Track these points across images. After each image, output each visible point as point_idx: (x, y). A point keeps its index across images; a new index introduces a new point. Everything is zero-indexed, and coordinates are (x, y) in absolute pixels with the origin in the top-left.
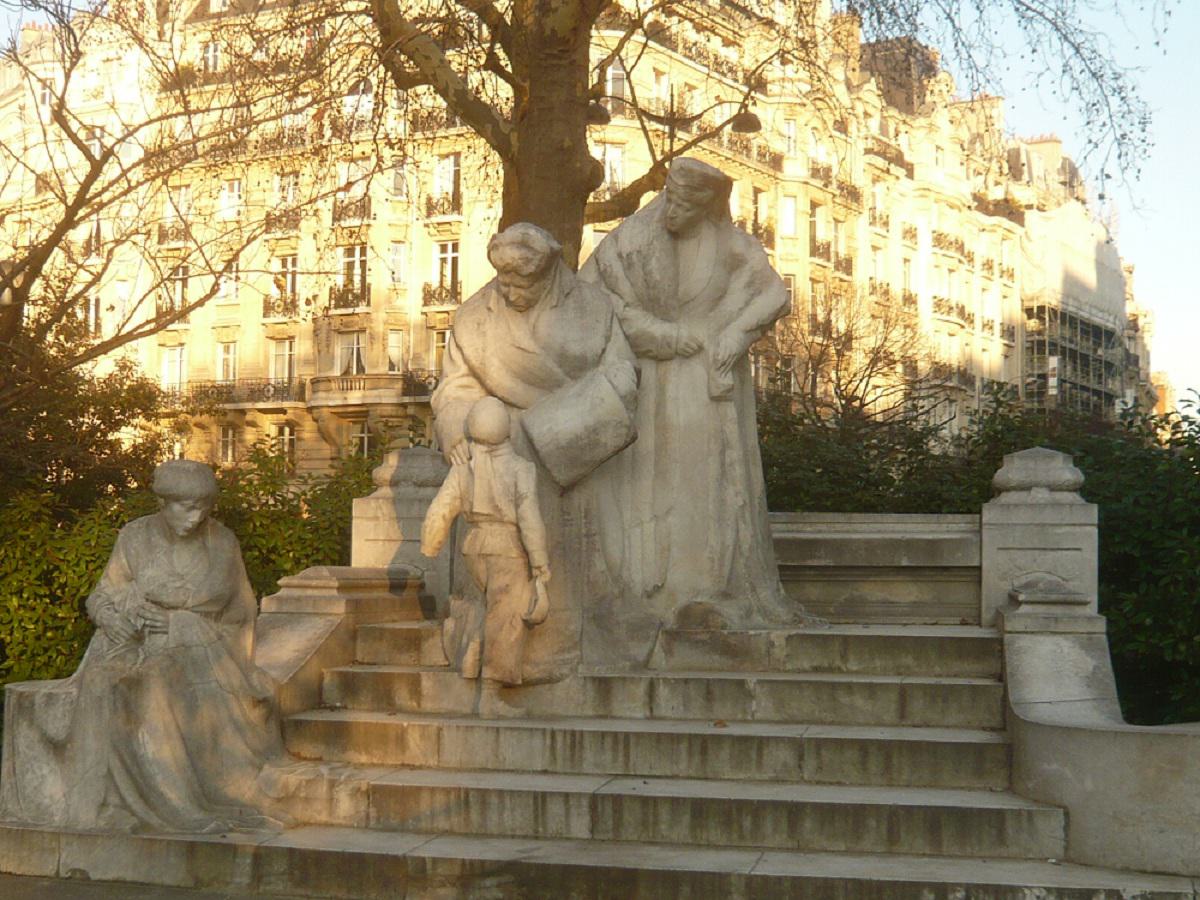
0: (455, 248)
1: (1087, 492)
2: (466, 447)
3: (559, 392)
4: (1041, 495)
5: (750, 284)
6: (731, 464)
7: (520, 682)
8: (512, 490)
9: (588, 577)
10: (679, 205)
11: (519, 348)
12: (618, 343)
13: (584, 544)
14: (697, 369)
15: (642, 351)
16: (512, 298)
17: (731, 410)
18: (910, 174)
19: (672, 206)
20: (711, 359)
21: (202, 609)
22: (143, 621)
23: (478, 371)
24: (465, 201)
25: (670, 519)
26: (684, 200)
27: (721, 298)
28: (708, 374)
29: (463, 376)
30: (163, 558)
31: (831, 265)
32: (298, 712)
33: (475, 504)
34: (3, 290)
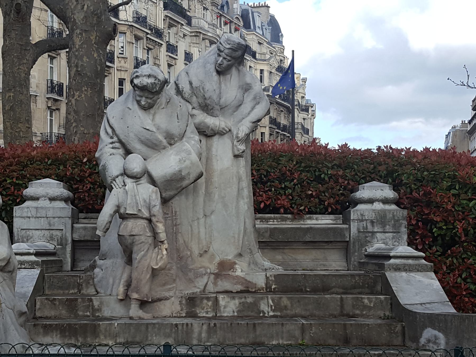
1: (360, 150)
2: (122, 181)
4: (378, 206)
5: (255, 98)
6: (242, 189)
7: (150, 300)
8: (148, 201)
9: (176, 246)
10: (224, 58)
12: (191, 128)
13: (175, 229)
14: (226, 140)
15: (206, 133)
16: (143, 103)
17: (242, 161)
19: (221, 58)
20: (235, 136)
23: (123, 141)
25: (213, 217)
26: (227, 55)
27: (240, 105)
28: (233, 144)
33: (128, 208)
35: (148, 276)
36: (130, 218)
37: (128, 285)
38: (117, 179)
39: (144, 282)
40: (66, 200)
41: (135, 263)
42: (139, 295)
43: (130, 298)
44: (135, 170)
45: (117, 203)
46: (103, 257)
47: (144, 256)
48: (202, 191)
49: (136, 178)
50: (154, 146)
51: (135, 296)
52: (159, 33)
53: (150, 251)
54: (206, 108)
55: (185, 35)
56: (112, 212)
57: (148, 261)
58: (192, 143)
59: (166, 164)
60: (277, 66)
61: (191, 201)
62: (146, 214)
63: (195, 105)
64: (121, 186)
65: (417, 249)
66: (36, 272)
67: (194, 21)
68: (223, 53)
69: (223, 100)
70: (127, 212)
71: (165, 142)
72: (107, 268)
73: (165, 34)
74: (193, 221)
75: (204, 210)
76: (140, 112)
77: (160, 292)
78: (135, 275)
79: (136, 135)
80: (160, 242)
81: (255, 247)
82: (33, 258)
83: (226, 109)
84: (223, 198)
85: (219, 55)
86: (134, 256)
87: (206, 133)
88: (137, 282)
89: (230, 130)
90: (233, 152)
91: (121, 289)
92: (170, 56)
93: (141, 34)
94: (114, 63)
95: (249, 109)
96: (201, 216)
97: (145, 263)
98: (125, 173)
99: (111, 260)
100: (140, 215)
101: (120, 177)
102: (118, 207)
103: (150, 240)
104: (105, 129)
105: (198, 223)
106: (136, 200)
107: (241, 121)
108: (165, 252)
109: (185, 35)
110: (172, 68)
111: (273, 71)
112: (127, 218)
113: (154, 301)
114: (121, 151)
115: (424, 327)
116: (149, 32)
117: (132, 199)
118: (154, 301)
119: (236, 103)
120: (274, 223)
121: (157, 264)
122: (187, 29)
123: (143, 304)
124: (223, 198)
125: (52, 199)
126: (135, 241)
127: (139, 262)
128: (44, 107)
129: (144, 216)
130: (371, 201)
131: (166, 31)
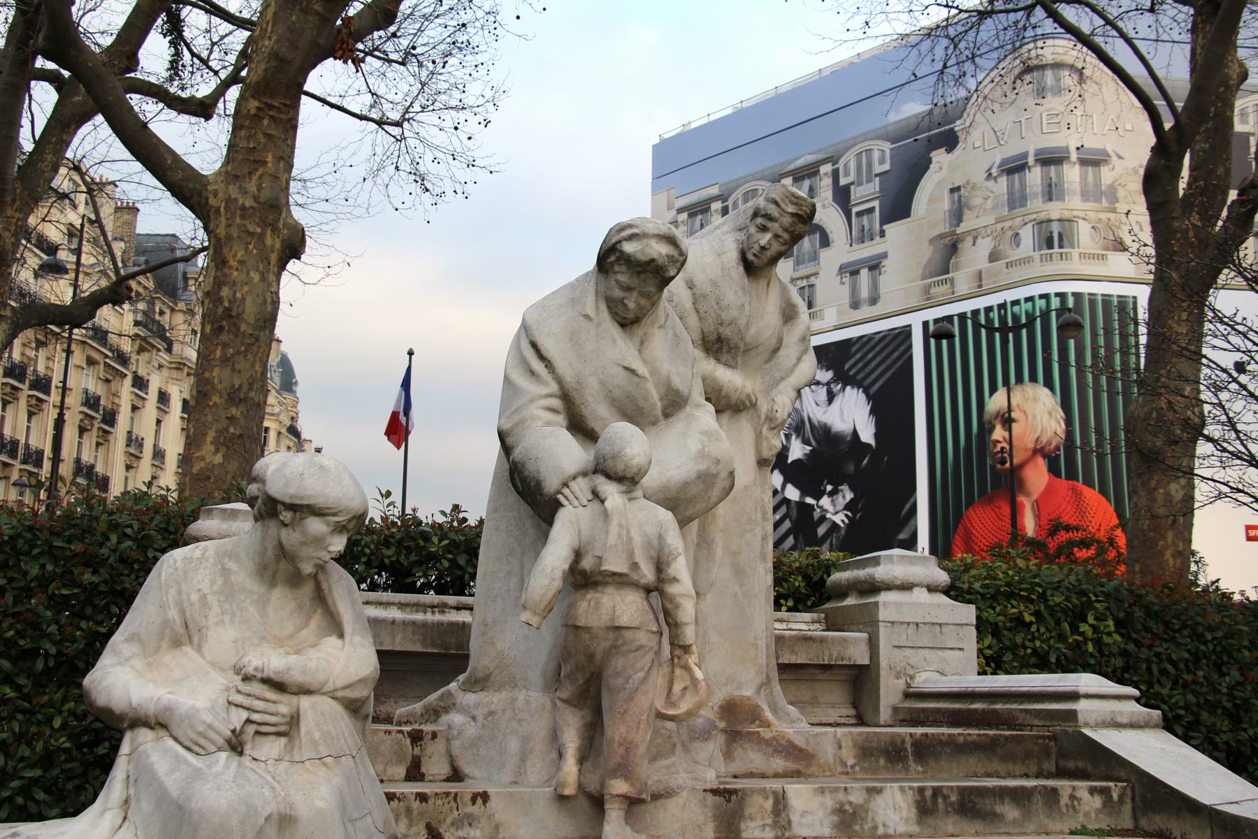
4: (920, 595)
8: (655, 543)
11: (626, 368)
18: (169, 350)
19: (768, 236)
21: (340, 694)
22: (245, 715)
29: (551, 396)
30: (252, 610)
31: (99, 417)
34: (18, 92)
36: (606, 584)
38: (573, 484)
42: (632, 785)
45: (576, 545)
46: (479, 683)
52: (123, 359)
53: (654, 670)
55: (160, 366)
57: (650, 695)
60: (288, 423)
64: (585, 503)
67: (176, 348)
68: (776, 225)
69: (753, 331)
70: (603, 568)
72: (492, 713)
73: (132, 361)
76: (614, 330)
79: (602, 383)
80: (680, 647)
81: (775, 674)
83: (753, 353)
84: (735, 554)
90: (758, 451)
92: (137, 395)
93: (96, 356)
94: (48, 394)
95: (794, 361)
99: (504, 694)
100: (634, 576)
101: (580, 479)
102: (578, 555)
106: (630, 539)
107: (776, 383)
109: (160, 366)
110: (138, 413)
111: (284, 431)
116: (110, 354)
117: (620, 536)
118: (656, 797)
122: (164, 357)
124: (735, 554)
126: (620, 642)
130: (906, 587)
131: (134, 357)
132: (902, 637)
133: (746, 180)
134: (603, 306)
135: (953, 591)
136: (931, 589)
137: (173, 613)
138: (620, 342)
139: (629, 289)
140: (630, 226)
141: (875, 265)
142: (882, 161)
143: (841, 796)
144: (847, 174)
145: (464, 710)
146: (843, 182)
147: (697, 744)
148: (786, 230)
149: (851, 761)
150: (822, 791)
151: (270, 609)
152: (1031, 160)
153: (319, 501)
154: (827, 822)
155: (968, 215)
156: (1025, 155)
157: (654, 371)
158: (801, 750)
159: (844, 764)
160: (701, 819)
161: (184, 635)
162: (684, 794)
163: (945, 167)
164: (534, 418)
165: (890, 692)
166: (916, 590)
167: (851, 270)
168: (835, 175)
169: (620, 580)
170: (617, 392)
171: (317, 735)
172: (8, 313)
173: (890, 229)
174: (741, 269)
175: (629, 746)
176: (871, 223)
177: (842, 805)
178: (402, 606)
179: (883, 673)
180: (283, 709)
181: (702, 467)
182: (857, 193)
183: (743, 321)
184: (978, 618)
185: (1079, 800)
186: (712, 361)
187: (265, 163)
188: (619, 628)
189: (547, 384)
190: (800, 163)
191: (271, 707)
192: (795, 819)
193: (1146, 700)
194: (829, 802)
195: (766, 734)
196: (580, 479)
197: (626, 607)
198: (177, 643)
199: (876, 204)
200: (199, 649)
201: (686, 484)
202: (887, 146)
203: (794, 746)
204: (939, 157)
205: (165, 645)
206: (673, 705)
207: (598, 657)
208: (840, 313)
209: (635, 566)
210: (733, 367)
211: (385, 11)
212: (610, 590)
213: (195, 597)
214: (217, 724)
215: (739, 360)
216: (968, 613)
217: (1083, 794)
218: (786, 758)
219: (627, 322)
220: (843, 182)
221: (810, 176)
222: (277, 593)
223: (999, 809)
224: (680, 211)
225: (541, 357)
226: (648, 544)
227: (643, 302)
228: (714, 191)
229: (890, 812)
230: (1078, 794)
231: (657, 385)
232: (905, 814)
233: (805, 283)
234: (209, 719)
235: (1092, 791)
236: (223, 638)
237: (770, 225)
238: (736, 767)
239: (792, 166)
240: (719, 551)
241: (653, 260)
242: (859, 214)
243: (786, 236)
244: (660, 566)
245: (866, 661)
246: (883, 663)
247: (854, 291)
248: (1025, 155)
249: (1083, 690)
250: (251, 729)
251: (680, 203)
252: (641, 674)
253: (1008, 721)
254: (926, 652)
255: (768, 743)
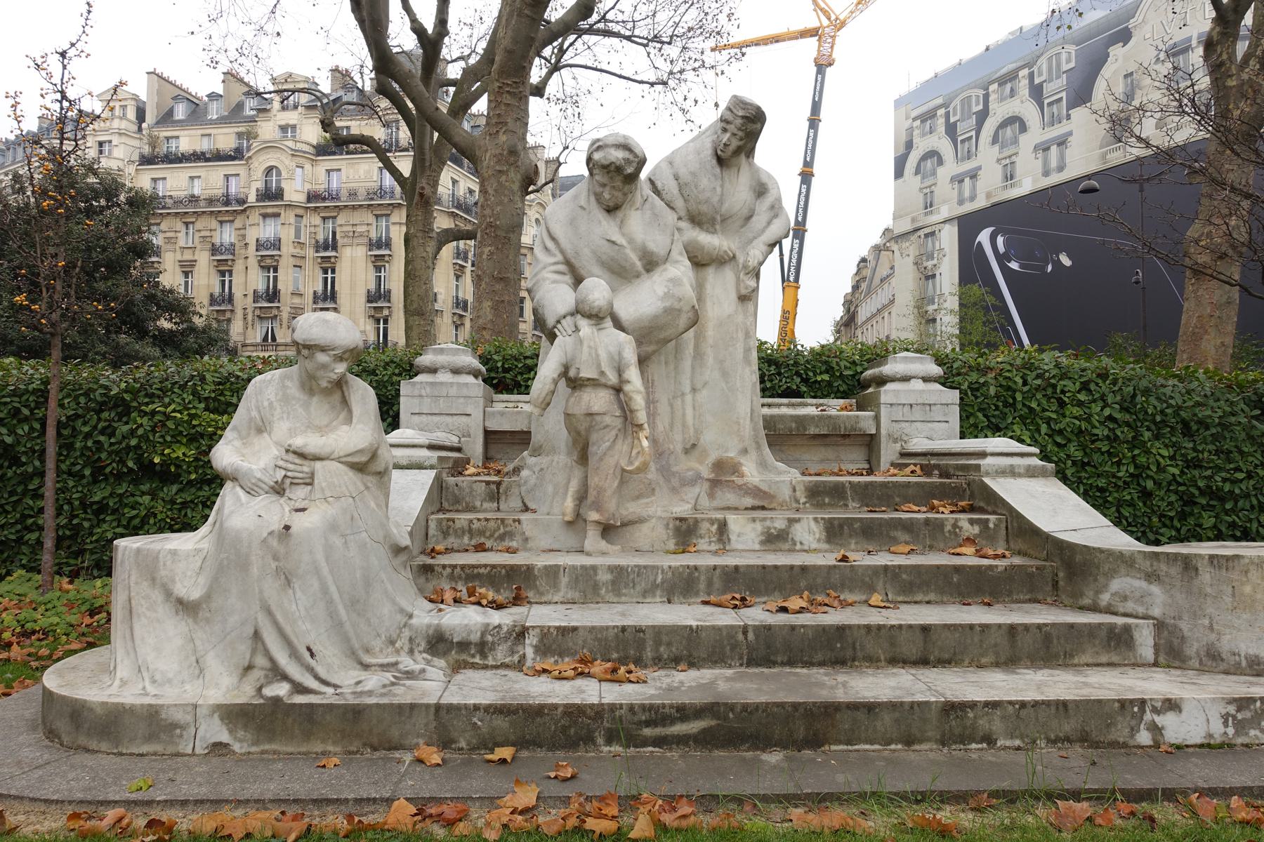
0: (333, 271)
3: (637, 281)
4: (917, 385)
8: (616, 357)
10: (734, 135)
12: (678, 249)
14: (728, 274)
19: (728, 135)
21: (349, 459)
22: (283, 473)
24: (339, 245)
25: (705, 392)
27: (751, 217)
30: (300, 410)
32: (1122, 561)
35: (616, 484)
37: (581, 498)
38: (563, 322)
39: (609, 492)
40: (476, 374)
41: (592, 461)
43: (585, 521)
44: (596, 304)
45: (564, 361)
46: (537, 452)
47: (610, 448)
48: (689, 350)
49: (596, 317)
50: (620, 273)
51: (594, 516)
53: (620, 442)
54: (696, 220)
56: (556, 376)
58: (680, 269)
59: (641, 301)
61: (672, 367)
62: (612, 378)
63: (683, 213)
65: (1021, 441)
66: (428, 477)
69: (726, 206)
71: (639, 264)
74: (674, 397)
75: (692, 382)
76: (600, 215)
77: (633, 509)
78: (594, 481)
79: (594, 252)
82: (425, 453)
83: (729, 221)
85: (725, 130)
86: (592, 449)
87: (700, 261)
88: (599, 493)
89: (734, 257)
90: (738, 290)
91: (569, 504)
96: (688, 389)
97: (610, 461)
98: (578, 311)
100: (603, 380)
101: (568, 318)
102: (566, 368)
103: (618, 423)
104: (543, 242)
105: (683, 401)
106: (598, 356)
107: (751, 241)
108: (645, 443)
112: (582, 386)
113: (624, 525)
114: (568, 278)
115: (1112, 574)
118: (624, 525)
119: (745, 212)
120: (785, 409)
121: (631, 463)
123: (607, 530)
124: (722, 362)
125: (456, 371)
127: (601, 459)
128: (450, 321)
129: (610, 383)
130: (906, 379)
132: (898, 414)
133: (962, 90)
134: (593, 199)
135: (945, 382)
136: (926, 379)
137: (254, 413)
138: (604, 223)
139: (604, 185)
140: (598, 140)
141: (1062, 142)
142: (1068, 61)
143: (768, 523)
144: (1040, 74)
145: (530, 468)
146: (1037, 81)
147: (686, 489)
148: (739, 129)
149: (803, 500)
150: (754, 520)
151: (312, 409)
152: (1194, 43)
153: (322, 342)
154: (757, 540)
155: (1138, 93)
156: (1190, 39)
157: (631, 241)
158: (765, 493)
159: (797, 501)
160: (665, 537)
161: (261, 428)
162: (654, 520)
163: (1120, 61)
164: (544, 279)
165: (888, 453)
166: (913, 381)
167: (1044, 148)
168: (1031, 76)
169: (594, 383)
170: (604, 257)
171: (324, 484)
172: (434, 235)
173: (1075, 113)
174: (714, 162)
175: (601, 490)
176: (1059, 110)
177: (769, 528)
178: (788, 405)
179: (883, 440)
180: (306, 469)
181: (668, 304)
182: (1047, 89)
183: (715, 199)
184: (961, 399)
185: (960, 529)
186: (698, 229)
187: (506, 123)
188: (591, 414)
189: (554, 255)
190: (1004, 71)
191: (299, 468)
192: (733, 537)
193: (1044, 457)
194: (759, 527)
195: (739, 481)
196: (568, 318)
197: (598, 400)
198: (260, 431)
199: (1064, 94)
200: (270, 434)
201: (656, 317)
202: (1072, 49)
203: (760, 490)
204: (1116, 51)
205: (253, 432)
206: (631, 463)
207: (583, 433)
208: (1034, 181)
209: (602, 373)
210: (714, 232)
211: (585, 7)
212: (589, 389)
213: (266, 404)
214: (266, 480)
215: (718, 227)
216: (955, 395)
217: (965, 525)
218: (754, 498)
219: (611, 210)
220: (1037, 81)
221: (1010, 80)
222: (315, 399)
223: (892, 534)
224: (914, 119)
225: (553, 239)
226: (611, 358)
227: (619, 194)
228: (939, 101)
229: (806, 535)
230: (960, 524)
231: (634, 250)
232: (817, 536)
233: (1008, 161)
234: (259, 475)
235: (972, 522)
236: (281, 428)
237: (728, 127)
238: (716, 503)
239: (998, 75)
240: (710, 360)
241: (612, 163)
242: (1050, 104)
243: (740, 134)
244: (620, 372)
245: (874, 432)
246: (883, 432)
247: (1046, 162)
248: (1190, 39)
249: (989, 450)
250: (288, 481)
251: (914, 114)
252: (608, 444)
253: (945, 473)
254: (918, 424)
255: (740, 487)
